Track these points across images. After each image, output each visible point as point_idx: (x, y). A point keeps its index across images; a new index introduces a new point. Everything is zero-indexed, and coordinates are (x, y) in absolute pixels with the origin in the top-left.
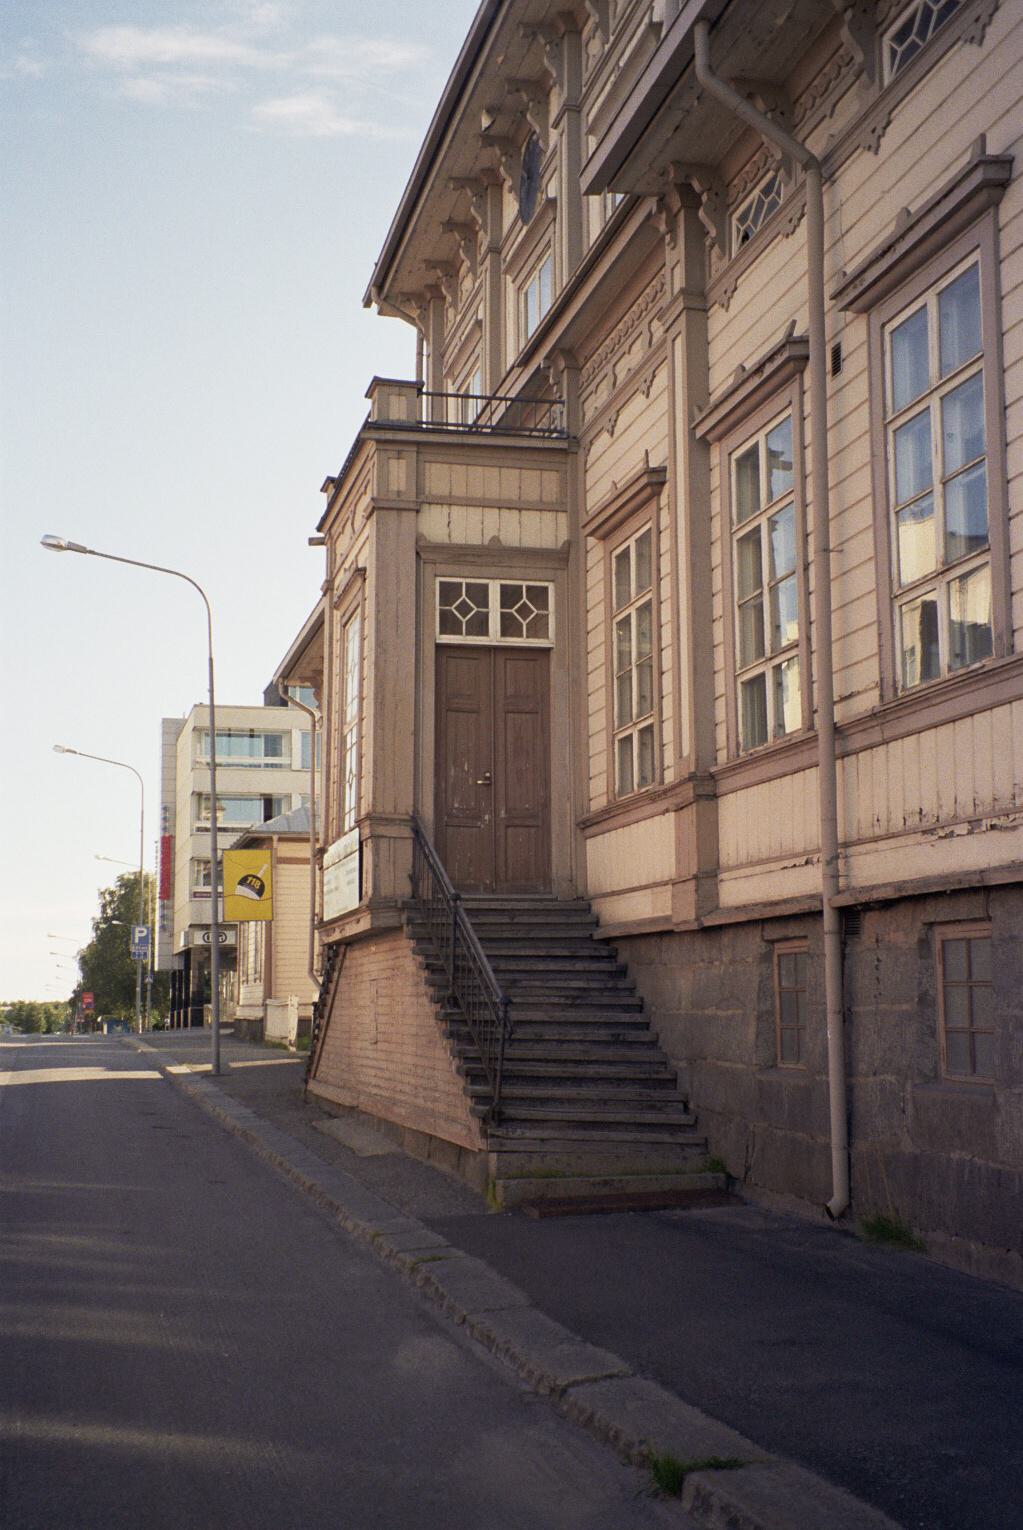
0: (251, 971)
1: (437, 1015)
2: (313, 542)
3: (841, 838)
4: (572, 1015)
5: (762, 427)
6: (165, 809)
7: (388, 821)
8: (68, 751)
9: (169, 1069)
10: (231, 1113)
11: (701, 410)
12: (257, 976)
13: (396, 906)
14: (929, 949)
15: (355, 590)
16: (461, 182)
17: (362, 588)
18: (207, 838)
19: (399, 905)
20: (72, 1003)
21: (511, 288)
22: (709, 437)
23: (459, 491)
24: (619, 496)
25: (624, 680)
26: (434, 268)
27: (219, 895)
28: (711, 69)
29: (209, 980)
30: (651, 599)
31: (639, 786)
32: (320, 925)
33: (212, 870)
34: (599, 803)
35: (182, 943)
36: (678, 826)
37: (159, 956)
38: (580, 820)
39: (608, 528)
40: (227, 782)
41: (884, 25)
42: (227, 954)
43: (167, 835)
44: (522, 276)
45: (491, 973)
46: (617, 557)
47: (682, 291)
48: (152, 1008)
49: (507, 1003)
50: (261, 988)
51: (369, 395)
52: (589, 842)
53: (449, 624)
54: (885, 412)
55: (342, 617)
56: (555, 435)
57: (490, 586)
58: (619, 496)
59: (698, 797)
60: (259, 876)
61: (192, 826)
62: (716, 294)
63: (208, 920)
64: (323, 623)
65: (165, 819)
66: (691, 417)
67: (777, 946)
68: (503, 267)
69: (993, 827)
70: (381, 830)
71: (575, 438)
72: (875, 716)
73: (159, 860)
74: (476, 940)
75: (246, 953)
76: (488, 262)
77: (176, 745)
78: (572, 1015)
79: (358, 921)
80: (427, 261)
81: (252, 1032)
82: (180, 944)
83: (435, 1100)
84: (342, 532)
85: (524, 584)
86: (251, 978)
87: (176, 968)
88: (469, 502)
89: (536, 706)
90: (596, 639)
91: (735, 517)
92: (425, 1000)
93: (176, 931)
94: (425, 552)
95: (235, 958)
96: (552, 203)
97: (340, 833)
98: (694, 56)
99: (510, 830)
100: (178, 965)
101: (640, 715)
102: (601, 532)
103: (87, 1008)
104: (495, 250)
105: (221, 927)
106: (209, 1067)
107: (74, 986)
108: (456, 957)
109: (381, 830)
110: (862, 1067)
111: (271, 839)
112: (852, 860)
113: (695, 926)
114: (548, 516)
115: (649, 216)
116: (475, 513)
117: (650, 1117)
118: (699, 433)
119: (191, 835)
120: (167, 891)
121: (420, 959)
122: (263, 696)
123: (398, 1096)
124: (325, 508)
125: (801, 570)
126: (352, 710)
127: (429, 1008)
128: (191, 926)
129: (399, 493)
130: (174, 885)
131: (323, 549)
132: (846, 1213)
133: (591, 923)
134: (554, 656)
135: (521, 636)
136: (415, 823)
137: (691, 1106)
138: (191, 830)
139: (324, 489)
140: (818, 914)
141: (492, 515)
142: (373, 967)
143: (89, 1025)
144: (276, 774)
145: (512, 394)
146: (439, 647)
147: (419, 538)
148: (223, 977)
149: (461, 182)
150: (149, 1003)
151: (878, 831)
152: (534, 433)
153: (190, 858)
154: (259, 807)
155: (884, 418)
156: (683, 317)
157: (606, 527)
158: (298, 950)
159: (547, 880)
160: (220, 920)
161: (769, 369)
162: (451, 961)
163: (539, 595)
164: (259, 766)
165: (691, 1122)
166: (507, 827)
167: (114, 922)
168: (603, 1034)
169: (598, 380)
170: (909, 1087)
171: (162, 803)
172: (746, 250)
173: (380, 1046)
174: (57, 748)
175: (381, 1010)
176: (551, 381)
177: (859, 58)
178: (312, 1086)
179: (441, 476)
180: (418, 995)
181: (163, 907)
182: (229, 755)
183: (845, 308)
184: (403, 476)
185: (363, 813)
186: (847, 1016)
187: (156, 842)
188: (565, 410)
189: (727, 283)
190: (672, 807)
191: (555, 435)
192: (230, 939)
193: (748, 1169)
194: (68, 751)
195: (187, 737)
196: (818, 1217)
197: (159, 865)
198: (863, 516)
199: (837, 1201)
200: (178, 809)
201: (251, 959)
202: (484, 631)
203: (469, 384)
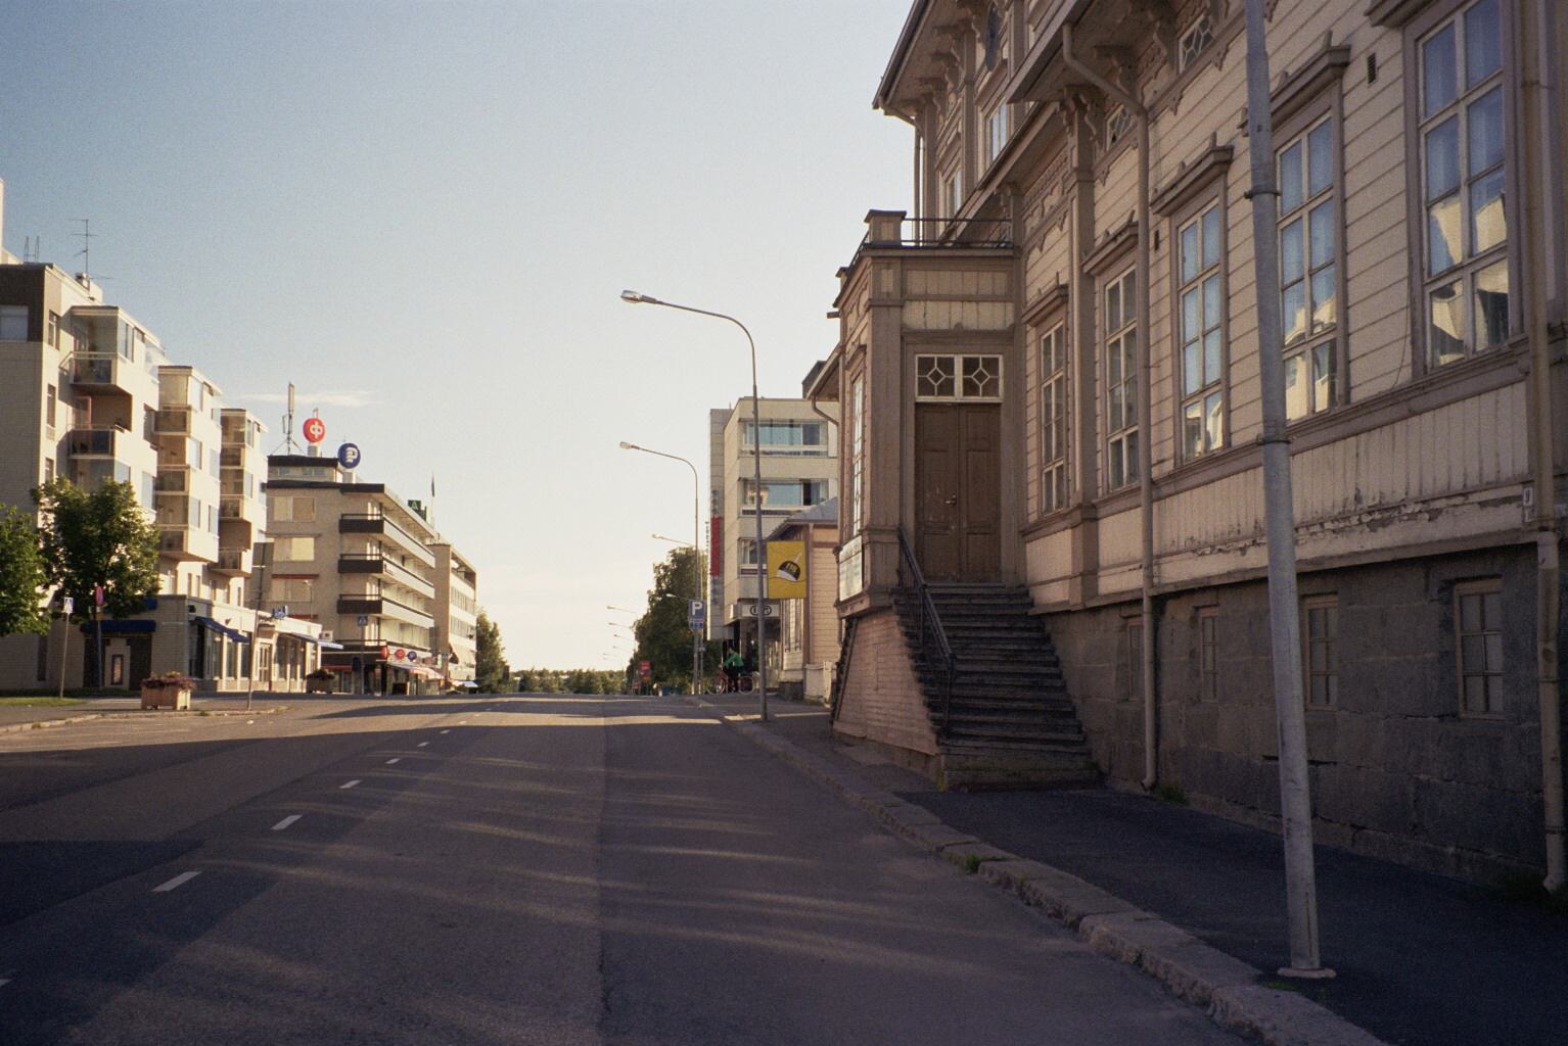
0: (792, 640)
1: (912, 666)
2: (830, 315)
3: (1155, 551)
4: (1008, 668)
5: (1199, 210)
6: (714, 492)
7: (882, 531)
8: (633, 447)
9: (727, 717)
10: (776, 744)
11: (1086, 254)
12: (798, 644)
13: (887, 592)
14: (1197, 621)
15: (858, 361)
16: (944, 29)
17: (864, 359)
18: (753, 520)
19: (889, 590)
20: (631, 670)
21: (981, 116)
22: (1092, 273)
23: (933, 290)
24: (1042, 300)
25: (1048, 430)
26: (927, 83)
27: (763, 572)
28: (1074, 56)
29: (756, 650)
30: (1134, 329)
31: (1057, 507)
32: (839, 604)
33: (756, 549)
34: (1033, 518)
35: (732, 616)
36: (1073, 535)
37: (711, 627)
38: (1022, 529)
39: (1039, 321)
40: (770, 469)
41: (1181, 32)
42: (772, 626)
43: (716, 516)
44: (990, 105)
45: (946, 640)
46: (1110, 290)
47: (1076, 170)
48: (705, 676)
49: (953, 657)
50: (801, 655)
51: (867, 220)
52: (1028, 545)
53: (925, 388)
54: (1178, 284)
55: (852, 375)
56: (1003, 245)
58: (1042, 300)
59: (1084, 520)
60: (796, 562)
61: (739, 509)
62: (1098, 173)
63: (755, 594)
64: (838, 364)
66: (1081, 259)
67: (1130, 620)
68: (975, 99)
69: (1220, 550)
71: (1019, 247)
72: (1171, 477)
73: (710, 539)
74: (937, 616)
75: (788, 626)
76: (964, 90)
77: (723, 433)
78: (1008, 668)
79: (862, 602)
80: (921, 79)
81: (795, 692)
82: (730, 616)
83: (912, 725)
84: (851, 312)
85: (981, 356)
86: (793, 646)
87: (727, 637)
88: (938, 298)
89: (989, 445)
90: (1032, 397)
91: (1107, 329)
92: (905, 657)
93: (726, 603)
94: (908, 336)
95: (779, 629)
96: (1005, 62)
97: (851, 538)
98: (1062, 44)
99: (970, 536)
100: (728, 635)
101: (1057, 457)
102: (1034, 321)
103: (644, 675)
104: (970, 82)
105: (766, 602)
106: (758, 716)
107: (631, 655)
108: (924, 627)
109: (876, 538)
110: (1164, 696)
111: (807, 526)
112: (1163, 567)
114: (999, 306)
115: (1054, 114)
116: (944, 306)
117: (1052, 735)
118: (1086, 269)
119: (739, 517)
120: (718, 568)
121: (903, 629)
122: (801, 386)
123: (891, 726)
124: (839, 291)
125: (1338, 261)
126: (858, 447)
127: (908, 663)
128: (739, 600)
129: (888, 294)
130: (723, 562)
131: (837, 321)
132: (1153, 787)
133: (1028, 604)
134: (1003, 407)
135: (978, 395)
136: (900, 532)
137: (1084, 729)
138: (739, 513)
139: (838, 275)
141: (957, 307)
142: (875, 635)
143: (645, 690)
144: (812, 460)
145: (970, 217)
146: (918, 405)
147: (903, 326)
148: (769, 646)
149: (944, 29)
150: (702, 671)
151: (1174, 549)
152: (986, 245)
153: (737, 538)
154: (799, 491)
155: (1178, 287)
156: (1076, 187)
157: (1038, 318)
158: (829, 626)
159: (997, 570)
160: (765, 596)
161: (1120, 240)
162: (921, 631)
163: (991, 365)
164: (799, 453)
165: (1081, 739)
166: (968, 534)
167: (669, 595)
168: (1027, 681)
169: (1033, 208)
170: (1184, 707)
171: (712, 486)
172: (1116, 147)
173: (880, 691)
175: (880, 666)
176: (1002, 204)
177: (1165, 52)
178: (838, 726)
179: (917, 280)
180: (902, 654)
181: (714, 582)
182: (772, 443)
183: (1158, 212)
184: (891, 280)
185: (865, 524)
186: (1157, 665)
187: (707, 523)
188: (1011, 225)
189: (1104, 165)
190: (1069, 526)
191: (1003, 245)
192: (775, 612)
193: (1111, 768)
194: (633, 447)
195: (733, 427)
196: (1139, 791)
197: (709, 544)
198: (1166, 348)
199: (1148, 779)
200: (726, 492)
201: (792, 630)
202: (951, 392)
203: (953, 181)
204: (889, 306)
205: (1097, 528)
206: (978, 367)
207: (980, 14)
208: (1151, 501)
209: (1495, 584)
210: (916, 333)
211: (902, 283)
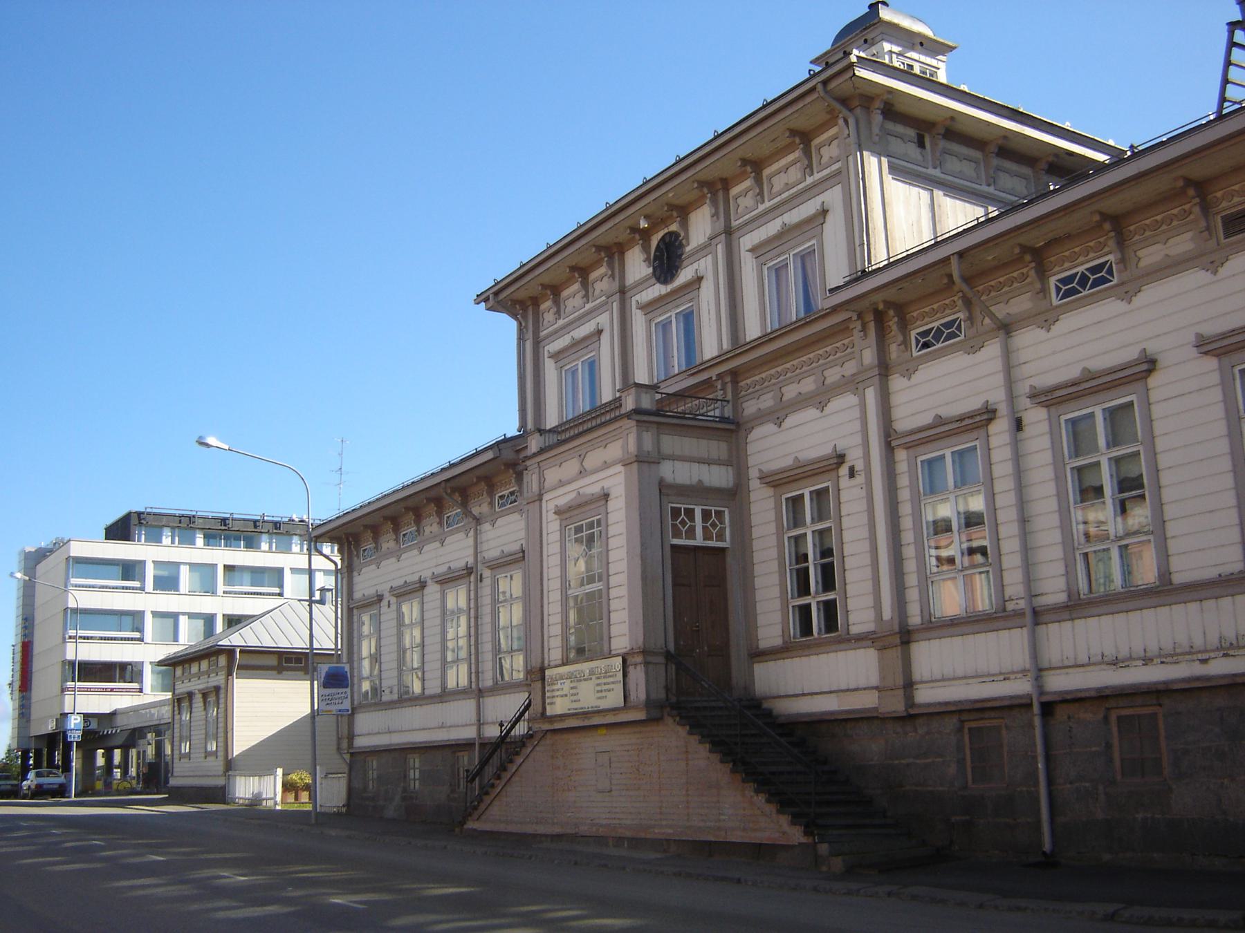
43: (26, 640)
53: (677, 534)
57: (696, 510)
65: (25, 628)
67: (966, 723)
69: (1162, 663)
94: (664, 488)
109: (650, 659)
113: (905, 714)
114: (723, 468)
130: (31, 680)
140: (1030, 705)
146: (673, 546)
163: (719, 514)
204: (649, 462)
205: (909, 649)
206: (681, 515)
207: (645, 241)
208: (1036, 624)
209: (466, 753)
210: (671, 486)
211: (658, 443)
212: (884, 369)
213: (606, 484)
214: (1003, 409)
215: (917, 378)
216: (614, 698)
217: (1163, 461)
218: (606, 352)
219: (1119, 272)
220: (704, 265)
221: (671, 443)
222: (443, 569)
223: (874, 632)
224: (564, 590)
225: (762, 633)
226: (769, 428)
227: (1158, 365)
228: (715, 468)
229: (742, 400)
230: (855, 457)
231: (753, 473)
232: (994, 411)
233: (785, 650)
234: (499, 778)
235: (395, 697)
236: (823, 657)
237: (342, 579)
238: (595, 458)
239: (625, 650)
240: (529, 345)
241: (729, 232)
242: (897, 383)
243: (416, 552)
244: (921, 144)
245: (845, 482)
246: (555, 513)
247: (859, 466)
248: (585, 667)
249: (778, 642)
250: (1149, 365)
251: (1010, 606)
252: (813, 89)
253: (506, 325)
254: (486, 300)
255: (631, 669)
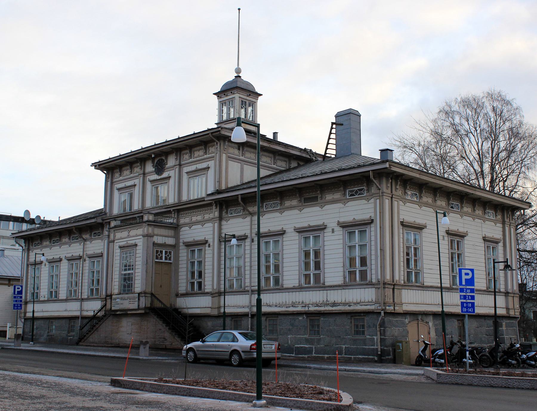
53: (157, 258)
70: (146, 295)
85: (168, 251)
94: (154, 244)
114: (172, 239)
163: (170, 253)
174: (342, 125)
202: (162, 259)
211: (153, 231)
212: (221, 218)
213: (136, 241)
214: (249, 236)
215: (229, 222)
216: (134, 306)
217: (285, 256)
218: (137, 192)
219: (280, 206)
220: (171, 173)
221: (157, 231)
222: (70, 255)
223: (211, 292)
224: (120, 271)
225: (180, 289)
226: (187, 228)
227: (286, 232)
228: (169, 238)
229: (180, 218)
230: (210, 241)
231: (181, 241)
232: (247, 236)
233: (186, 295)
234: (93, 329)
235: (46, 299)
236: (199, 298)
237: (25, 253)
238: (133, 232)
239: (139, 292)
240: (109, 183)
241: (180, 165)
242: (224, 222)
243: (58, 247)
244: (239, 149)
245: (207, 248)
246: (119, 247)
247: (211, 244)
248: (126, 296)
249: (184, 292)
250: (282, 233)
251: (246, 288)
252: (208, 134)
253: (101, 176)
254: (95, 166)
255: (141, 298)
